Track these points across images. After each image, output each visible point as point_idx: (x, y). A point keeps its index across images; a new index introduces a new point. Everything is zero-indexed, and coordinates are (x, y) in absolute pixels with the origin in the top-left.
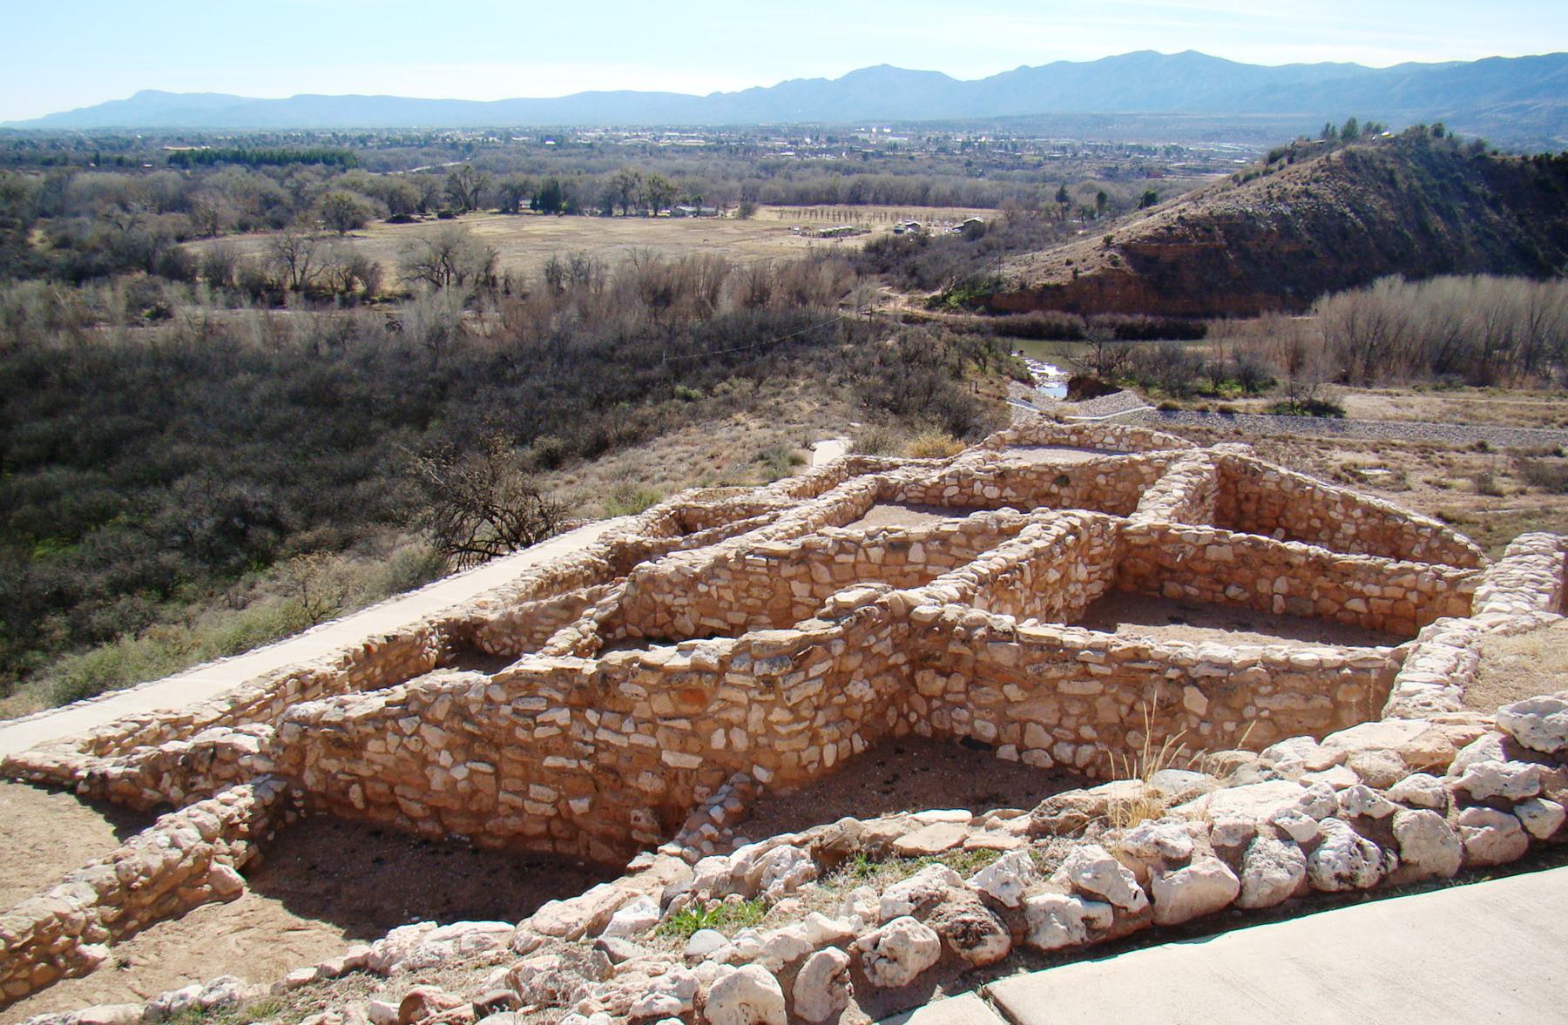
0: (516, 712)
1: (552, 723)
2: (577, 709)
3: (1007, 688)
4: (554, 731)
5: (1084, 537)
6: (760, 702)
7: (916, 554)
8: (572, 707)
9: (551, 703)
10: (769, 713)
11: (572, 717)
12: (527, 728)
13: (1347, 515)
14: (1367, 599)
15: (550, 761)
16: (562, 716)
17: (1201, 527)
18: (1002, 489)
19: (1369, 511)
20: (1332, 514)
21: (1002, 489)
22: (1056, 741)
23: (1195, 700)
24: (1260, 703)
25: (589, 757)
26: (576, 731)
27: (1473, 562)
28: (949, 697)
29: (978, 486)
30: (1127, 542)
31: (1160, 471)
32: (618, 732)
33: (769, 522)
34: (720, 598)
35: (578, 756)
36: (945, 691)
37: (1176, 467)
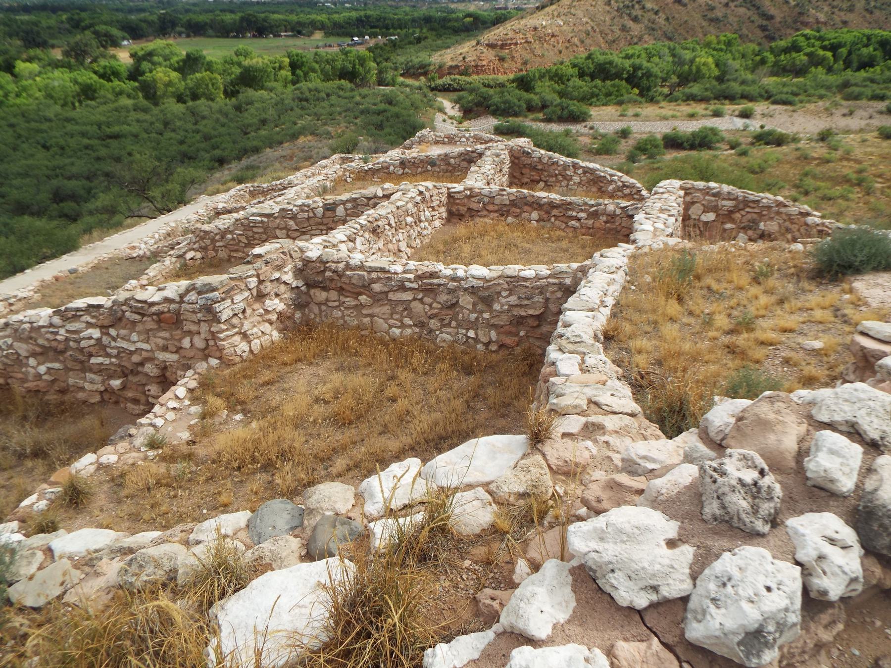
0: (68, 331)
1: (90, 338)
2: (104, 328)
3: (360, 298)
4: (92, 342)
5: (427, 195)
6: (204, 321)
7: (340, 211)
8: (102, 327)
9: (89, 325)
10: (211, 327)
11: (102, 333)
12: (75, 341)
13: (575, 173)
14: (579, 220)
15: (93, 360)
16: (96, 333)
17: (327, 197)
18: (404, 169)
19: (587, 171)
20: (568, 173)
21: (404, 169)
22: (391, 327)
23: (466, 300)
24: (503, 300)
25: (115, 357)
26: (106, 340)
27: (635, 195)
28: (331, 304)
29: (392, 168)
30: (453, 197)
31: (481, 155)
32: (129, 340)
33: (279, 196)
34: (240, 241)
35: (108, 355)
36: (327, 300)
37: (488, 153)
